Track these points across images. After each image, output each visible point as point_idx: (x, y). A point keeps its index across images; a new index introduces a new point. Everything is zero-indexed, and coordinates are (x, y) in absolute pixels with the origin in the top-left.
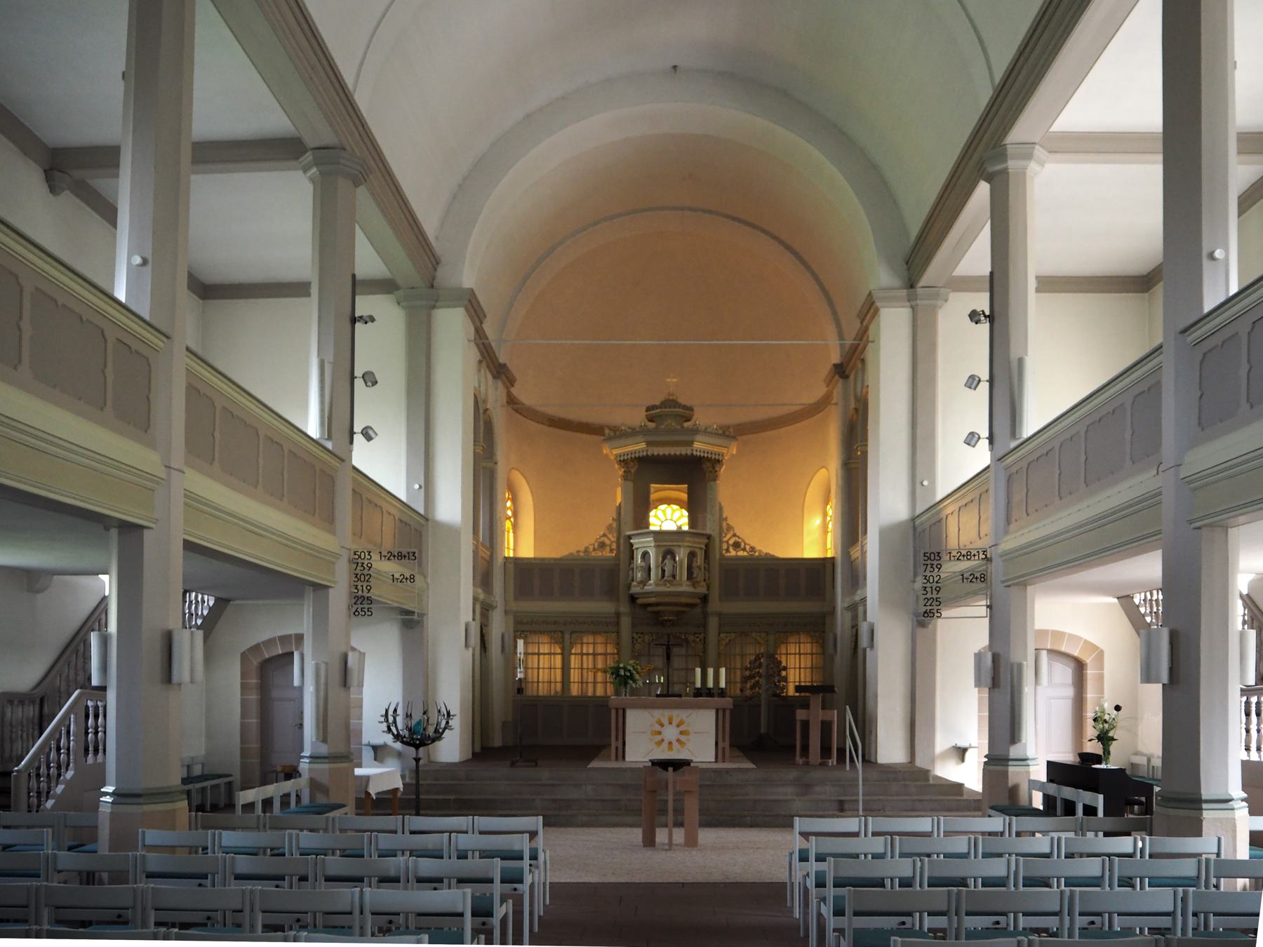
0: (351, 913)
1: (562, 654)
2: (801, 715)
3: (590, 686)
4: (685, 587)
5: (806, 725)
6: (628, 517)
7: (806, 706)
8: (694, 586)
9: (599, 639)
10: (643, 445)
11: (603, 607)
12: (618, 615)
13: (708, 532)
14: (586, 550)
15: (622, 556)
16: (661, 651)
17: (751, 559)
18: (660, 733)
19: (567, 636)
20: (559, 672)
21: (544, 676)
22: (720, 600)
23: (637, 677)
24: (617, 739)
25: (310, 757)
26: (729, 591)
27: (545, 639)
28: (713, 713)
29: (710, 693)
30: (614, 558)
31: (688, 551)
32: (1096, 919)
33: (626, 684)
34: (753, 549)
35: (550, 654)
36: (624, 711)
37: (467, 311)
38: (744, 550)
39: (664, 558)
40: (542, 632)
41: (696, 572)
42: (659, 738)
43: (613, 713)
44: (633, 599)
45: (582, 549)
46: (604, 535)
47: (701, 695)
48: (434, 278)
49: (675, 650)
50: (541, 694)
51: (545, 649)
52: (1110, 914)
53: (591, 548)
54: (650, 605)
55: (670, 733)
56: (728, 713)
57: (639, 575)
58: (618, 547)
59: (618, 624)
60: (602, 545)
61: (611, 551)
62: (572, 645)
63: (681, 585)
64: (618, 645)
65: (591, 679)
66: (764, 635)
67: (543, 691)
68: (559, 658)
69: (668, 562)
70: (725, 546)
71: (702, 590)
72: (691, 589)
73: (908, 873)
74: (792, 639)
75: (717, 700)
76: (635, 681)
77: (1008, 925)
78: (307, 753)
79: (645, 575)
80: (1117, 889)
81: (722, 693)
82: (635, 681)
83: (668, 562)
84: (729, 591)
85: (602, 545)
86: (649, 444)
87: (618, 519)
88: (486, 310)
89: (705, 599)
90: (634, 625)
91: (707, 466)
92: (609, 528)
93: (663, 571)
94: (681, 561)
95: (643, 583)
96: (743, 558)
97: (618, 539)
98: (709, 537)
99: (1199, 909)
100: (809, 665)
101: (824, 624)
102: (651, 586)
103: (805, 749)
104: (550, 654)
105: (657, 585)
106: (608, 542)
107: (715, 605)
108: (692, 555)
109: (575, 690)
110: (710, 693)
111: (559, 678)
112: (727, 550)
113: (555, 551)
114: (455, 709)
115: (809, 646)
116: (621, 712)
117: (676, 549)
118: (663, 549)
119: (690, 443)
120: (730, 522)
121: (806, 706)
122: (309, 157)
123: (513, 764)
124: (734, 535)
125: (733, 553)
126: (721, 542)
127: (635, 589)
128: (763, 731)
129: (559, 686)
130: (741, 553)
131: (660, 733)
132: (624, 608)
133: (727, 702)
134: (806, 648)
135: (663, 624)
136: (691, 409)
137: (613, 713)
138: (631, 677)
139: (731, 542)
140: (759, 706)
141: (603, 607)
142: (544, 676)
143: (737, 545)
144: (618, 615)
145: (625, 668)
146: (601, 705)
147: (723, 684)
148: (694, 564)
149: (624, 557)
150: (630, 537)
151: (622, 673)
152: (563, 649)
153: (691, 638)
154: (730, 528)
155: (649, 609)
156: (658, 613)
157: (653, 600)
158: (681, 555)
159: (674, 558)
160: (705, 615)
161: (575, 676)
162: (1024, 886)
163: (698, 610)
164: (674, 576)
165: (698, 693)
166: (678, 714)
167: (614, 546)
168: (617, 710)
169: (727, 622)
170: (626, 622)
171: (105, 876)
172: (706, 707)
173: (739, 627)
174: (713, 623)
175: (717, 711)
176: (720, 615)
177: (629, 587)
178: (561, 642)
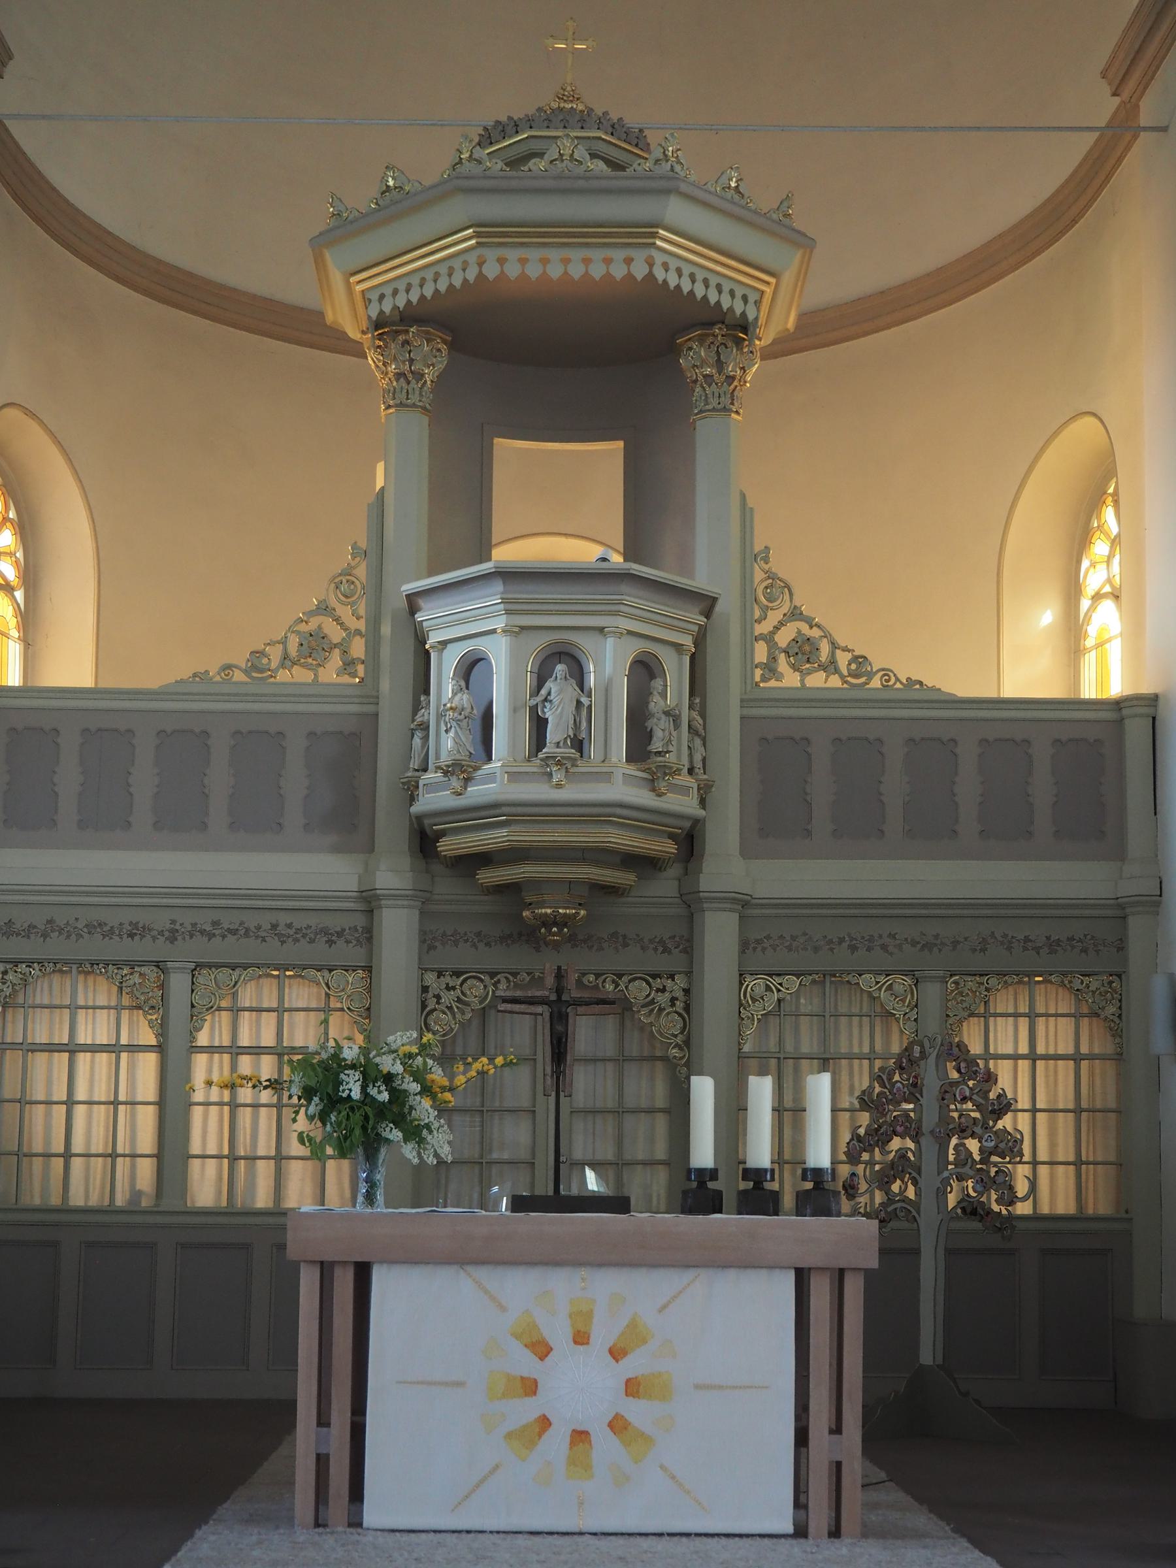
1: (160, 1048)
3: (264, 1170)
4: (618, 784)
6: (408, 530)
8: (652, 784)
9: (301, 994)
10: (465, 241)
11: (318, 872)
12: (369, 903)
13: (701, 581)
14: (256, 663)
15: (385, 685)
16: (523, 1032)
18: (530, 1387)
19: (179, 983)
20: (147, 1117)
21: (90, 1131)
22: (746, 852)
23: (424, 1109)
24: (323, 1421)
26: (777, 821)
27: (101, 991)
28: (786, 1284)
29: (758, 1196)
31: (633, 648)
33: (372, 1146)
35: (114, 1049)
36: (363, 1272)
38: (831, 667)
39: (541, 680)
40: (89, 967)
41: (660, 729)
42: (525, 1411)
43: (308, 1283)
44: (424, 839)
45: (241, 659)
46: (324, 609)
47: (713, 1204)
49: (587, 1034)
50: (77, 1199)
51: (95, 1028)
53: (275, 654)
54: (484, 859)
55: (581, 1386)
56: (854, 1289)
57: (448, 742)
59: (368, 936)
60: (315, 647)
61: (349, 665)
62: (195, 1015)
63: (607, 777)
65: (265, 1146)
66: (902, 983)
67: (85, 1188)
68: (148, 1063)
69: (559, 688)
70: (761, 653)
71: (684, 803)
72: (642, 797)
74: (1003, 1002)
75: (790, 1231)
76: (415, 1133)
79: (470, 742)
81: (819, 1194)
82: (415, 1133)
83: (559, 688)
84: (777, 821)
86: (490, 232)
87: (376, 552)
89: (690, 841)
90: (427, 942)
91: (695, 358)
92: (342, 580)
93: (540, 725)
95: (461, 771)
97: (375, 622)
98: (708, 604)
100: (1065, 1099)
101: (1121, 946)
102: (492, 784)
104: (114, 1049)
105: (514, 777)
106: (335, 634)
107: (727, 867)
108: (645, 670)
109: (205, 1187)
110: (758, 1196)
111: (146, 1141)
112: (770, 669)
113: (158, 667)
115: (1065, 1027)
116: (344, 1283)
117: (585, 642)
118: (541, 641)
119: (642, 233)
120: (777, 565)
124: (795, 614)
125: (790, 679)
126: (749, 640)
127: (435, 798)
128: (926, 1357)
129: (146, 1170)
130: (817, 680)
131: (530, 1387)
132: (393, 873)
133: (850, 1237)
134: (1058, 1035)
135: (530, 935)
137: (308, 1283)
138: (397, 1111)
139: (784, 638)
140: (917, 1252)
141: (318, 872)
142: (90, 1131)
143: (803, 652)
144: (369, 903)
145: (370, 1074)
146: (241, 1256)
147: (820, 1154)
148: (656, 704)
149: (392, 687)
150: (413, 603)
151: (352, 1086)
152: (162, 1030)
153: (638, 991)
154: (777, 586)
155: (488, 876)
156: (512, 889)
157: (497, 838)
158: (608, 663)
159: (578, 674)
160: (691, 905)
161: (205, 1131)
163: (665, 886)
164: (579, 745)
165: (698, 1194)
166: (621, 1296)
167: (358, 648)
168: (326, 1269)
169: (769, 934)
170: (397, 929)
172: (747, 1262)
173: (818, 951)
174: (720, 935)
175: (802, 1277)
176: (743, 905)
177: (411, 791)
178: (155, 1005)
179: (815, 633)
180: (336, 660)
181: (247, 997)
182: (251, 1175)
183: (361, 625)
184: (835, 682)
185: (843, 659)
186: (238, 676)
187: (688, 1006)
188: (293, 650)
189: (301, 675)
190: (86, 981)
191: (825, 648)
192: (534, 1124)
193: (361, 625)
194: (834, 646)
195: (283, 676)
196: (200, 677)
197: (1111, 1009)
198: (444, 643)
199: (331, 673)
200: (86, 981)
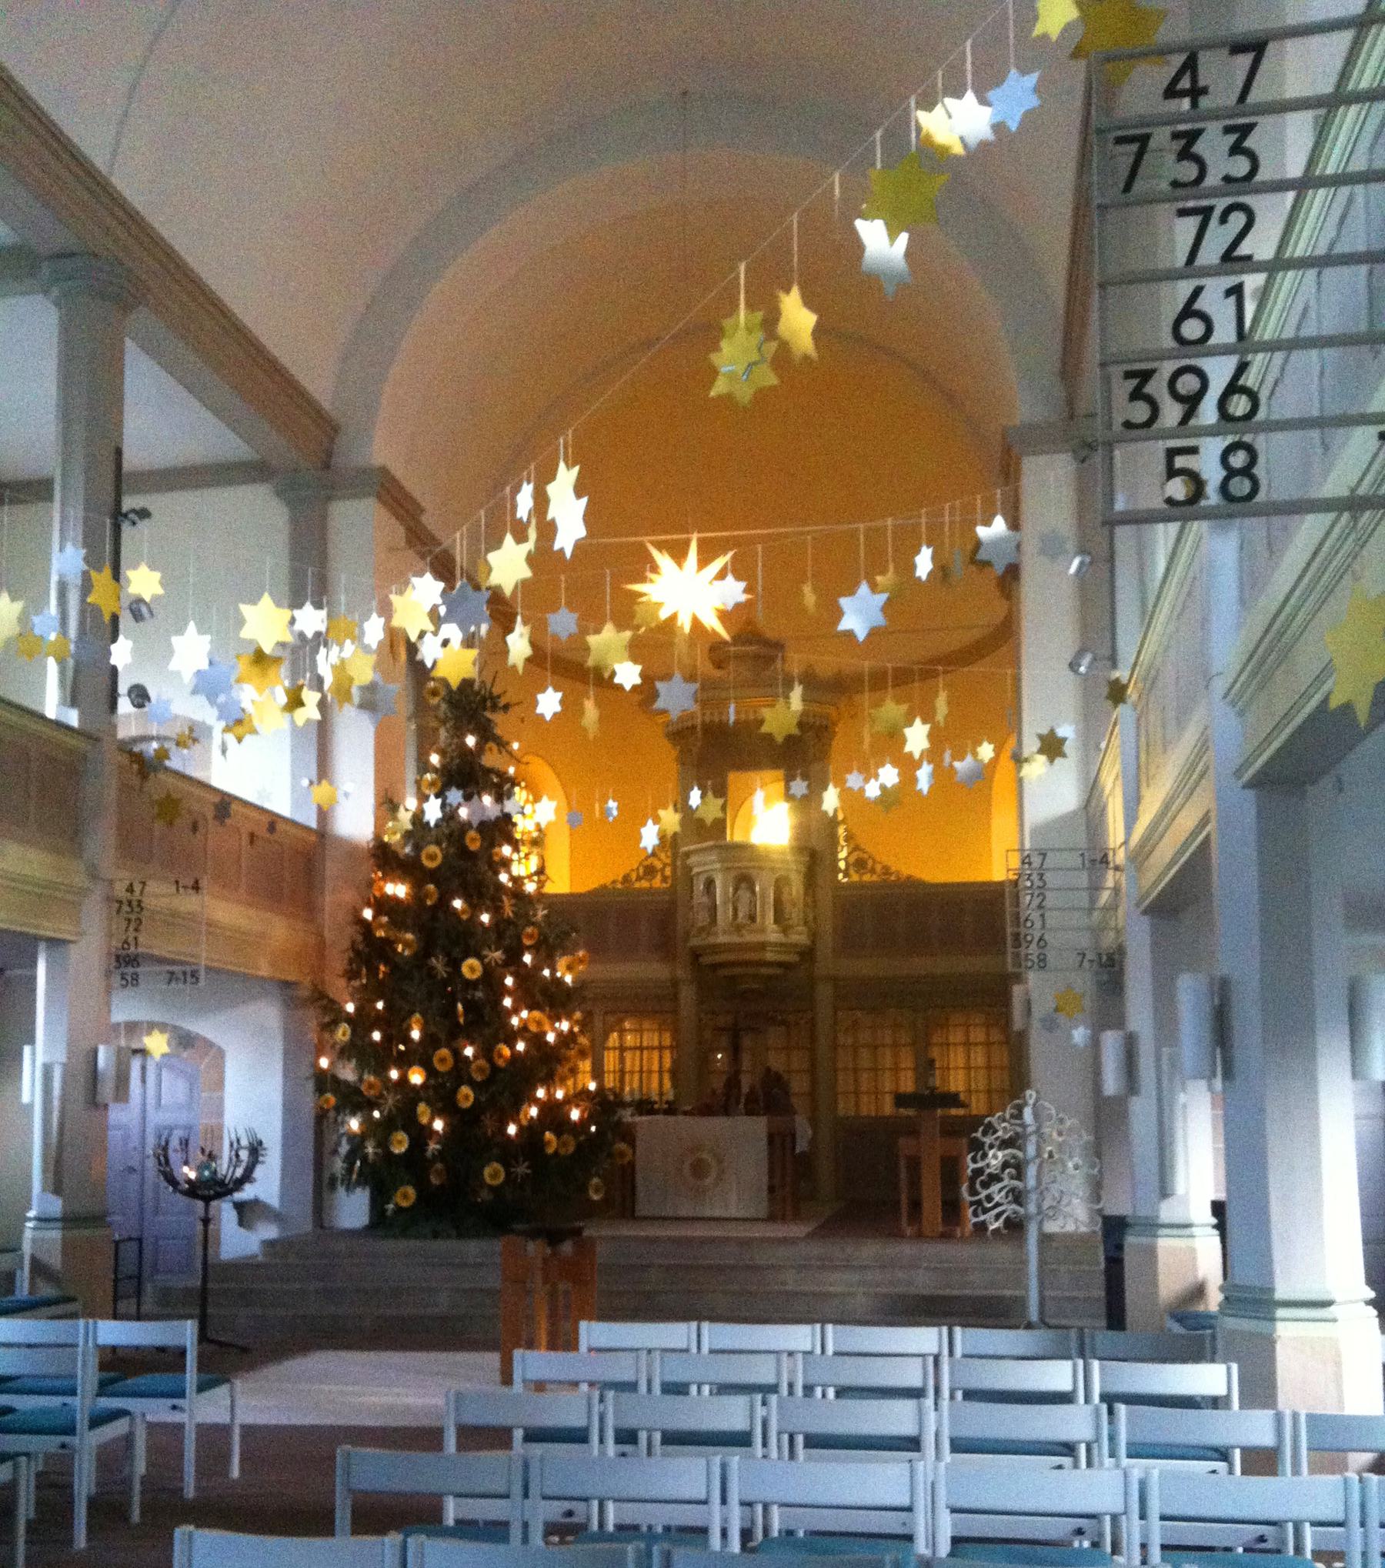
0: (705, 1502)
2: (905, 1145)
5: (914, 1164)
7: (913, 1131)
11: (651, 970)
14: (626, 879)
17: (885, 885)
25: (38, 1219)
30: (664, 892)
32: (579, 1507)
34: (886, 870)
37: (379, 497)
38: (873, 871)
48: (329, 454)
52: (766, 1507)
53: (634, 876)
54: (721, 965)
58: (674, 871)
59: (675, 997)
61: (664, 879)
64: (676, 1032)
72: (784, 940)
73: (1267, 1440)
77: (589, 1519)
78: (31, 1214)
80: (1125, 1462)
85: (650, 871)
88: (417, 494)
94: (763, 896)
96: (872, 885)
99: (750, 1498)
103: (916, 1205)
106: (659, 865)
114: (273, 1138)
118: (733, 873)
121: (913, 1131)
122: (46, 270)
123: (436, 1235)
127: (695, 942)
130: (867, 878)
136: (779, 646)
141: (651, 970)
144: (675, 983)
153: (791, 1018)
156: (733, 978)
162: (1129, 1456)
167: (668, 872)
170: (687, 994)
171: (518, 1434)
176: (834, 979)
179: (866, 856)
180: (659, 877)
181: (627, 1025)
182: (649, 1079)
183: (668, 861)
184: (875, 878)
185: (878, 868)
186: (619, 886)
187: (813, 1023)
188: (641, 871)
189: (645, 884)
190: (499, 697)
191: (870, 863)
192: (205, 1255)
193: (668, 861)
194: (874, 861)
195: (637, 885)
196: (604, 887)
197: (1003, 1022)
198: (699, 874)
199: (657, 882)
200: (499, 697)
